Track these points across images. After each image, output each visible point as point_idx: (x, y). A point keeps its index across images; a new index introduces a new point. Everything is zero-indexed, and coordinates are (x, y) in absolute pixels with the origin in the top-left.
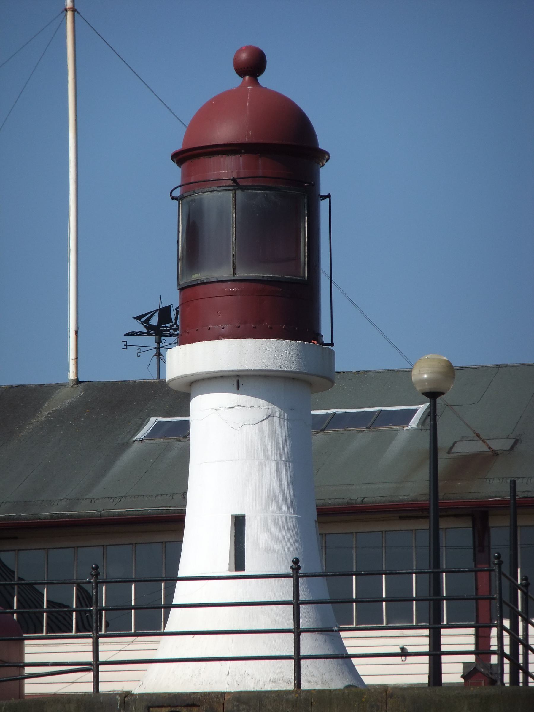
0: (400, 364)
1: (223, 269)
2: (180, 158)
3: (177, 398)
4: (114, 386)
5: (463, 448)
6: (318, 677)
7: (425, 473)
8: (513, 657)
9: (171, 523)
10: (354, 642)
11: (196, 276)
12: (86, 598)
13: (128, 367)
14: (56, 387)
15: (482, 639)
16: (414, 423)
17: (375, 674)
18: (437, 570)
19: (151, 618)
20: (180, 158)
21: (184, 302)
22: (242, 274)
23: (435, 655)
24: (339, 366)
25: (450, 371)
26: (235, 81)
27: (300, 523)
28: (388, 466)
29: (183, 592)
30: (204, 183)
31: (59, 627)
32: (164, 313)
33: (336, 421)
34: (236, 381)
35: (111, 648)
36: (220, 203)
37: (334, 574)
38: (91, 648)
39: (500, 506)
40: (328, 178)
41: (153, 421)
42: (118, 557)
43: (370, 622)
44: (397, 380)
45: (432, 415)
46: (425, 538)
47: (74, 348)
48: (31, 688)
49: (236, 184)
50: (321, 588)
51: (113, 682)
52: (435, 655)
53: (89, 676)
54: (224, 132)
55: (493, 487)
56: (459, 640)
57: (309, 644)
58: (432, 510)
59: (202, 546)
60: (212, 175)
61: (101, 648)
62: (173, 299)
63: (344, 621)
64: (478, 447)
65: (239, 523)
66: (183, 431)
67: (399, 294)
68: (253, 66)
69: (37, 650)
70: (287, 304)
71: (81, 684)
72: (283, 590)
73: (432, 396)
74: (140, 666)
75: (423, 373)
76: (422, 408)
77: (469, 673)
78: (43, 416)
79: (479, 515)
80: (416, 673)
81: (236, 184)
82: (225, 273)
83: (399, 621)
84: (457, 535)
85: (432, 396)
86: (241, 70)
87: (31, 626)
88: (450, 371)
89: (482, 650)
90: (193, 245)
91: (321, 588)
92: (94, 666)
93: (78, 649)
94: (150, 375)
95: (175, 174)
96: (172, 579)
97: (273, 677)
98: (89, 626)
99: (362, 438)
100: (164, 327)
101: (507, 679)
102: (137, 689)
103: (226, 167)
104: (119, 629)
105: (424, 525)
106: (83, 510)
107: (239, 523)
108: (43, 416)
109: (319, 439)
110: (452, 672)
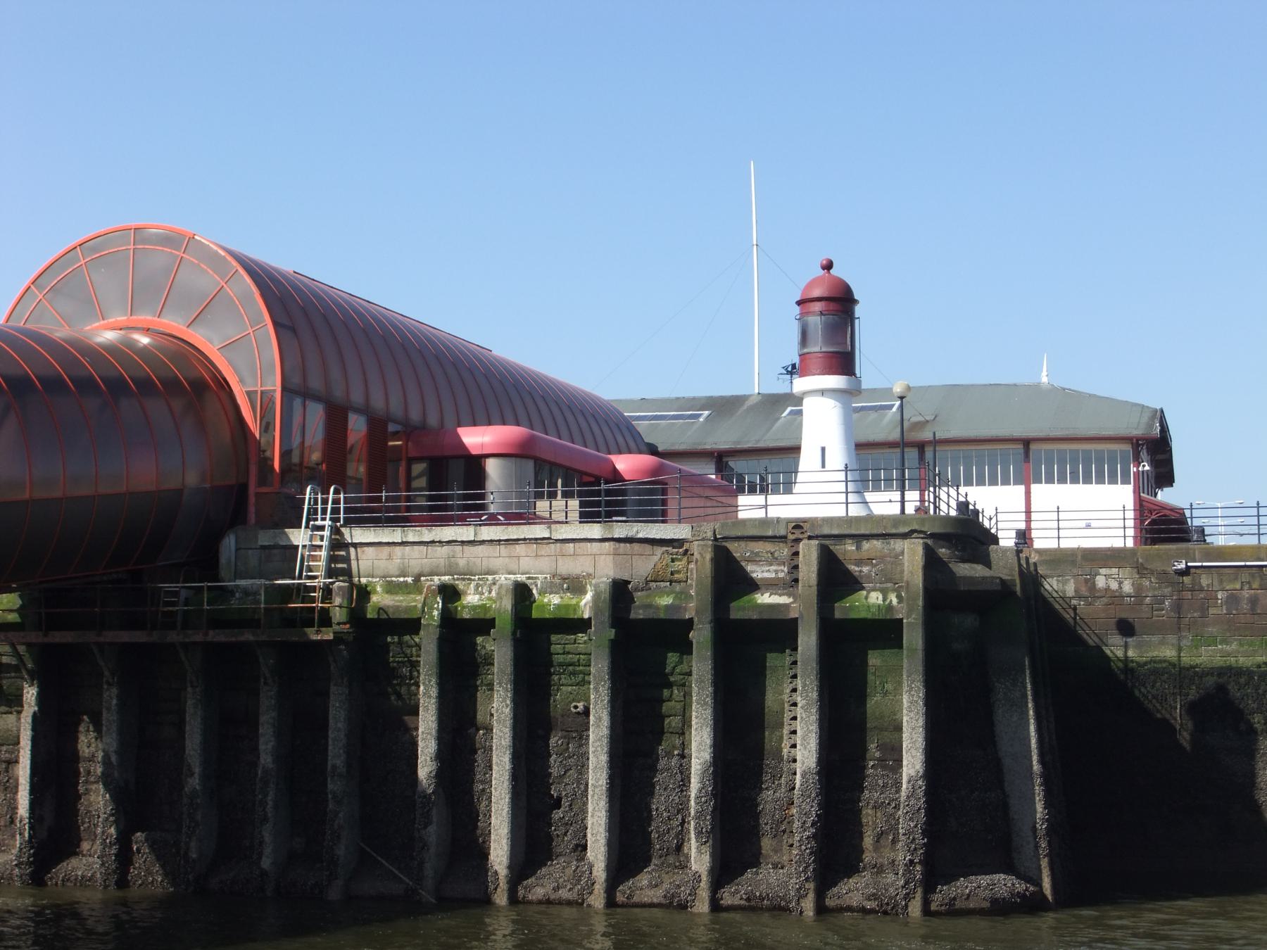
0: (887, 385)
1: (817, 346)
2: (799, 303)
3: (797, 400)
4: (774, 395)
5: (914, 419)
6: (856, 511)
7: (899, 430)
8: (934, 503)
9: (796, 450)
10: (869, 496)
11: (806, 350)
12: (762, 479)
13: (780, 387)
14: (750, 396)
15: (922, 495)
16: (894, 409)
17: (878, 510)
18: (58, 637)
19: (788, 488)
20: (799, 303)
21: (801, 361)
22: (824, 349)
23: (903, 502)
24: (864, 386)
25: (909, 388)
26: (822, 272)
27: (848, 449)
28: (884, 428)
29: (800, 477)
30: (808, 313)
31: (752, 491)
32: (794, 366)
33: (863, 408)
34: (823, 392)
35: (772, 499)
36: (815, 322)
37: (863, 470)
38: (1034, 516)
39: (930, 442)
40: (858, 311)
41: (789, 409)
42: (774, 463)
43: (877, 488)
44: (887, 392)
45: (901, 406)
46: (899, 455)
47: (756, 377)
48: (741, 515)
49: (821, 313)
50: (856, 475)
51: (774, 513)
52: (903, 502)
53: (784, 551)
54: (817, 293)
55: (926, 435)
56: (913, 496)
57: (852, 497)
58: (901, 444)
59: (808, 459)
60: (812, 309)
61: (1023, 517)
62: (797, 360)
63: (867, 489)
64: (920, 419)
65: (823, 449)
66: (800, 413)
67: (886, 357)
68: (828, 266)
69: (743, 500)
70: (843, 362)
71: (760, 514)
72: (842, 476)
73: (902, 398)
74: (782, 507)
75: (898, 389)
76: (898, 403)
77: (917, 510)
78: (745, 407)
79: (921, 446)
80: (895, 509)
81: (821, 313)
82: (817, 349)
83: (889, 488)
84: (912, 454)
85: (902, 398)
86: (823, 268)
87: (741, 490)
88: (909, 388)
89: (922, 500)
90: (804, 338)
91: (856, 475)
92: (766, 506)
93: (759, 499)
94: (788, 391)
95: (797, 309)
96: (796, 472)
97: (839, 512)
98: (764, 490)
99: (873, 415)
100: (792, 371)
101: (932, 512)
102: (782, 516)
103: (818, 307)
104: (776, 492)
105: (898, 450)
106: (761, 445)
107: (823, 449)
108: (745, 407)
109: (855, 416)
110: (910, 509)
